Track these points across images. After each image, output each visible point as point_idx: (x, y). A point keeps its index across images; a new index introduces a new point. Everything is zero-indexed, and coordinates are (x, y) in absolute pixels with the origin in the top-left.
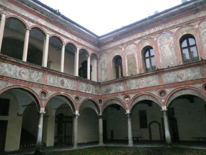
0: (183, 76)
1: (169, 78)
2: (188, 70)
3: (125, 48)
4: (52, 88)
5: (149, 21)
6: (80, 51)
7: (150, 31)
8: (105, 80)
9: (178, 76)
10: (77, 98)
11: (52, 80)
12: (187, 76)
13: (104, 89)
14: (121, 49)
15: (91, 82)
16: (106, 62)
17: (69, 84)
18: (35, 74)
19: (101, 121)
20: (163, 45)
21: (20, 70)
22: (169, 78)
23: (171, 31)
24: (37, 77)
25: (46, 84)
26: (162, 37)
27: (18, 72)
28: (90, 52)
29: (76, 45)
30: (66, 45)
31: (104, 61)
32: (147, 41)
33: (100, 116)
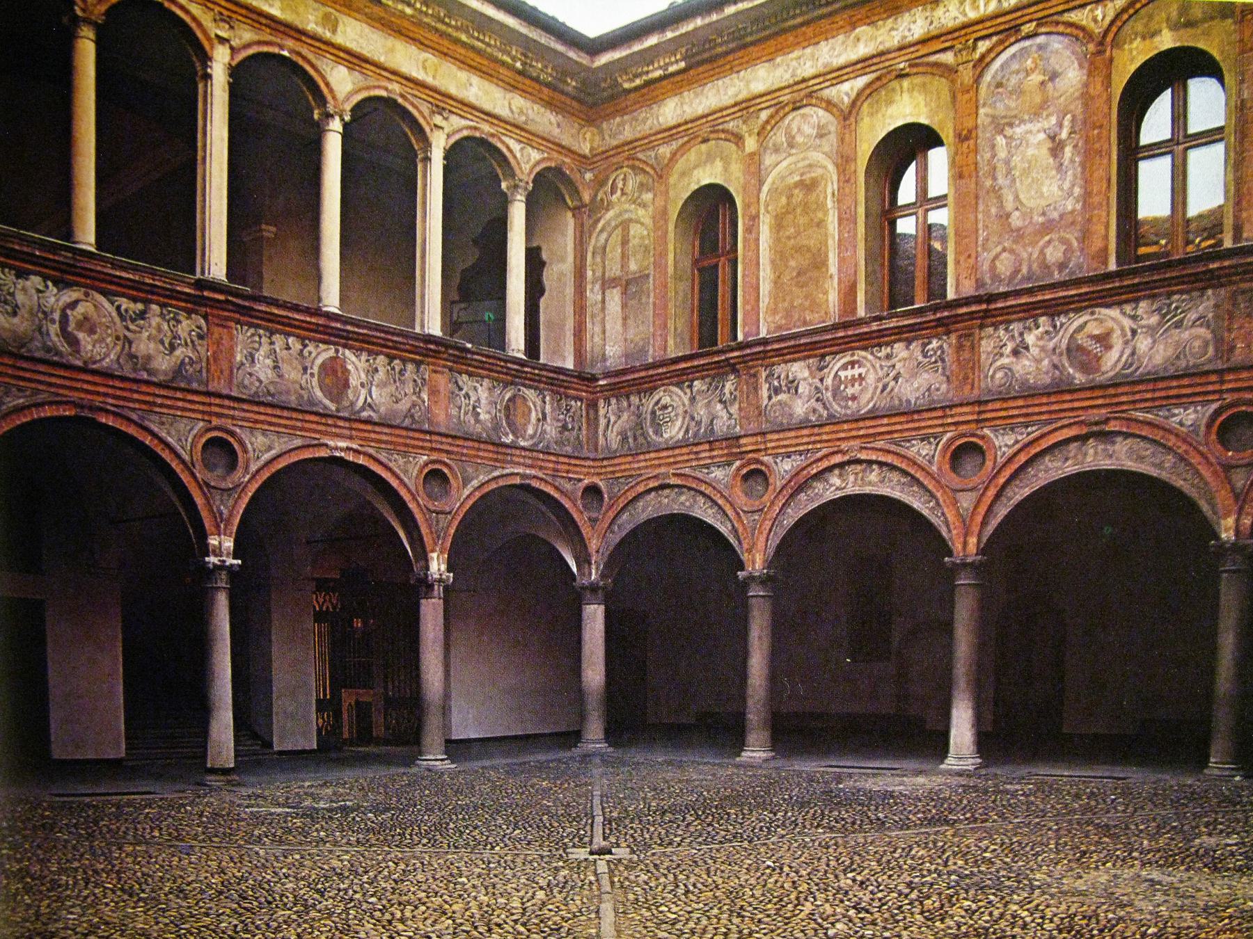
0: (1109, 347)
1: (1024, 355)
2: (1140, 312)
3: (761, 133)
4: (271, 406)
6: (449, 155)
8: (627, 356)
9: (1074, 350)
10: (435, 477)
11: (269, 362)
13: (613, 421)
14: (738, 139)
15: (530, 372)
16: (635, 230)
17: (372, 384)
18: (159, 330)
19: (594, 617)
21: (61, 303)
22: (1024, 355)
23: (1073, 17)
24: (172, 348)
27: (57, 316)
28: (528, 160)
29: (420, 109)
30: (347, 118)
31: (625, 225)
32: (911, 90)
33: (594, 588)
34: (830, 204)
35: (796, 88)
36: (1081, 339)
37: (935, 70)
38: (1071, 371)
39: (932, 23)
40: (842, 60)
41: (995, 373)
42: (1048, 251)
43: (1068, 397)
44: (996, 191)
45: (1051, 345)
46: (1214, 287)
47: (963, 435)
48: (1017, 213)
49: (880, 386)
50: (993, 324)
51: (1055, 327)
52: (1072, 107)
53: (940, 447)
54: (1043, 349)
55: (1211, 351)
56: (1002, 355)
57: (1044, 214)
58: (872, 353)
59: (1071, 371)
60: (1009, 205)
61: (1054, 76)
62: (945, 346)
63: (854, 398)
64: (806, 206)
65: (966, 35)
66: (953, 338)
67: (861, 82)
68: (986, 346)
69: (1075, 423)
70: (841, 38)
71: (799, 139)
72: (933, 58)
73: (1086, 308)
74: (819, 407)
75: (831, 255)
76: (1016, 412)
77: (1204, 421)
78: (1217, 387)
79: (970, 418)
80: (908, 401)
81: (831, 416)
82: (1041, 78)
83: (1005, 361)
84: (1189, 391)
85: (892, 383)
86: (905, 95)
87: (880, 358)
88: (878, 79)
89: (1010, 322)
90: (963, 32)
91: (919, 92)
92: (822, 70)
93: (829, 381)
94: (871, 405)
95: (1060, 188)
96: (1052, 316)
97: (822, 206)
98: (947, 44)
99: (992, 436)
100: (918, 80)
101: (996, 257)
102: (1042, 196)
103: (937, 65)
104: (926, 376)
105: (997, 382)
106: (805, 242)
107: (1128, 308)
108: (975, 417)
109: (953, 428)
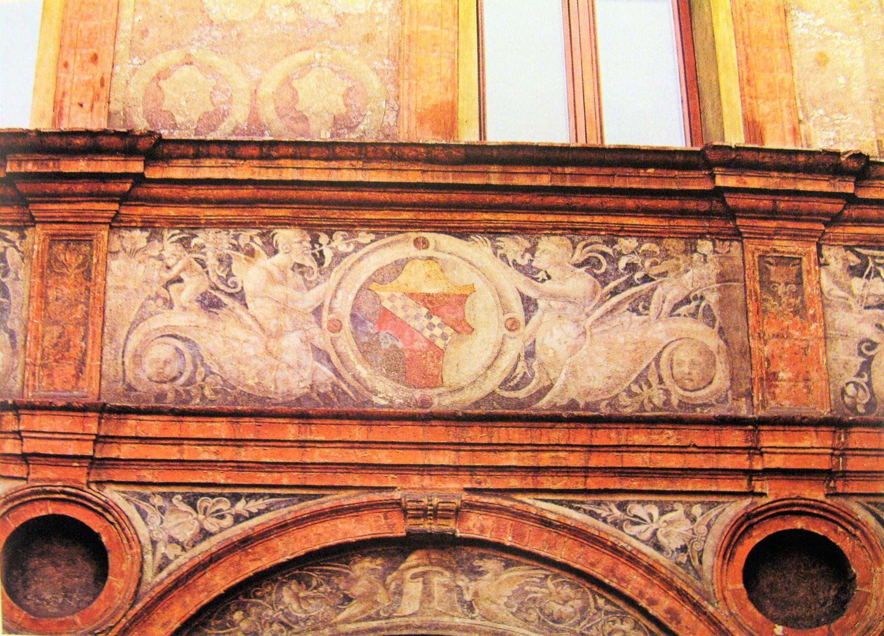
2: (541, 261)
12: (515, 347)
25: (763, 144)
36: (390, 297)
41: (146, 344)
45: (310, 299)
46: (715, 236)
47: (44, 495)
50: (147, 225)
51: (320, 259)
54: (284, 308)
55: (721, 379)
59: (363, 372)
66: (36, 237)
69: (372, 506)
73: (405, 226)
76: (205, 454)
77: (712, 543)
78: (742, 462)
79: (71, 449)
83: (178, 319)
84: (674, 461)
89: (195, 225)
96: (312, 230)
99: (130, 510)
107: (513, 246)
108: (87, 450)
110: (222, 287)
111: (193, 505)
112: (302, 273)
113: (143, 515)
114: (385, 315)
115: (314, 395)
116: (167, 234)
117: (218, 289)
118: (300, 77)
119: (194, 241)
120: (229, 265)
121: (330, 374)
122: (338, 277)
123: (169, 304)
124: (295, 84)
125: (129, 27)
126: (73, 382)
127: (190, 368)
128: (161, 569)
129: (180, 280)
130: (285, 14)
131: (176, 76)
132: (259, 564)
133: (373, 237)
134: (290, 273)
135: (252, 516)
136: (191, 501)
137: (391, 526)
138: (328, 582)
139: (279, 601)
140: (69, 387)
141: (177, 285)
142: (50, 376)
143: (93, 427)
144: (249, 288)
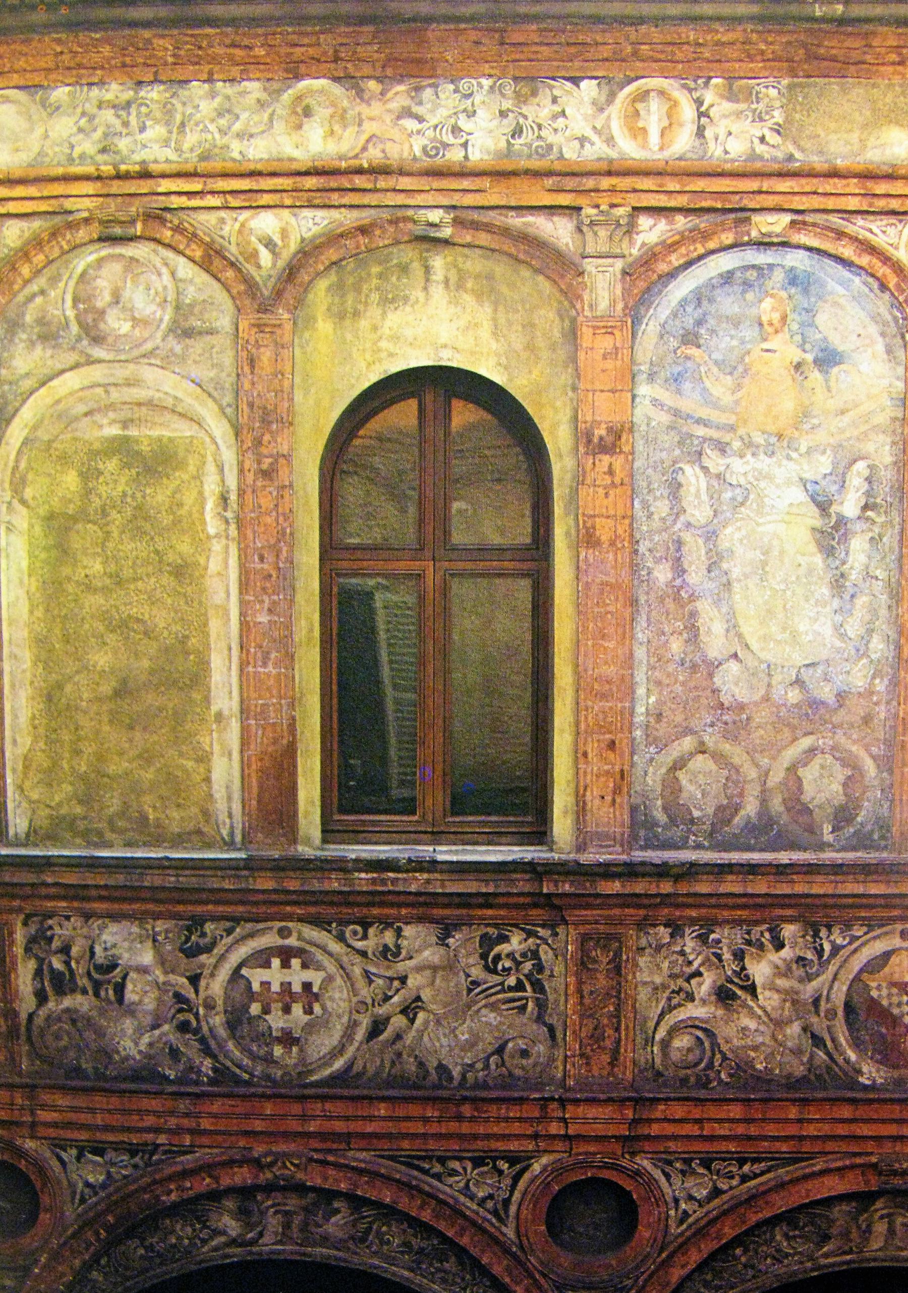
5: (544, 1169)
7: (539, 110)
20: (722, 448)
26: (728, 303)
32: (457, 284)
34: (213, 526)
35: (116, 187)
36: (878, 989)
37: (520, 251)
38: (852, 1056)
39: (517, 132)
40: (258, 151)
41: (673, 1031)
42: (808, 774)
43: (846, 1112)
44: (680, 598)
48: (733, 667)
49: (365, 1022)
51: (820, 952)
52: (870, 447)
53: (522, 1184)
56: (690, 997)
57: (798, 682)
58: (341, 938)
59: (852, 1056)
60: (715, 643)
61: (828, 359)
62: (546, 954)
63: (288, 1039)
64: (141, 521)
65: (613, 190)
67: (311, 223)
68: (648, 973)
70: (254, 88)
71: (117, 324)
72: (516, 221)
74: (190, 1050)
75: (217, 661)
80: (442, 1068)
81: (221, 1075)
82: (795, 354)
83: (696, 1011)
85: (398, 1021)
86: (438, 292)
87: (363, 954)
88: (363, 230)
90: (606, 183)
91: (479, 296)
92: (192, 161)
93: (216, 986)
94: (339, 1064)
95: (839, 630)
97: (185, 524)
98: (564, 200)
99: (658, 1174)
100: (474, 263)
101: (679, 765)
102: (795, 636)
103: (526, 239)
104: (492, 1017)
105: (675, 1056)
106: (143, 611)
109: (560, 1145)
110: (736, 980)
111: (708, 1168)
112: (804, 966)
113: (667, 1176)
114: (873, 1004)
115: (812, 1077)
116: (688, 931)
117: (732, 982)
118: (805, 765)
119: (712, 936)
120: (742, 959)
121: (825, 1057)
122: (835, 968)
123: (690, 997)
124: (800, 772)
125: (643, 710)
126: (608, 1068)
127: (708, 1054)
128: (682, 1222)
129: (700, 974)
130: (790, 694)
131: (691, 765)
132: (760, 1215)
133: (865, 929)
134: (794, 966)
135: (756, 1176)
136: (706, 1164)
137: (867, 1182)
138: (812, 1224)
139: (773, 1238)
140: (605, 1073)
141: (697, 979)
142: (588, 1064)
143: (629, 1114)
144: (759, 981)
